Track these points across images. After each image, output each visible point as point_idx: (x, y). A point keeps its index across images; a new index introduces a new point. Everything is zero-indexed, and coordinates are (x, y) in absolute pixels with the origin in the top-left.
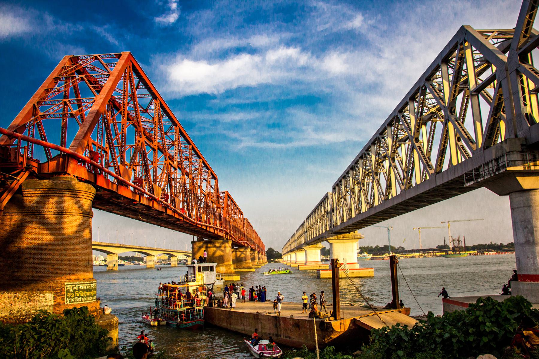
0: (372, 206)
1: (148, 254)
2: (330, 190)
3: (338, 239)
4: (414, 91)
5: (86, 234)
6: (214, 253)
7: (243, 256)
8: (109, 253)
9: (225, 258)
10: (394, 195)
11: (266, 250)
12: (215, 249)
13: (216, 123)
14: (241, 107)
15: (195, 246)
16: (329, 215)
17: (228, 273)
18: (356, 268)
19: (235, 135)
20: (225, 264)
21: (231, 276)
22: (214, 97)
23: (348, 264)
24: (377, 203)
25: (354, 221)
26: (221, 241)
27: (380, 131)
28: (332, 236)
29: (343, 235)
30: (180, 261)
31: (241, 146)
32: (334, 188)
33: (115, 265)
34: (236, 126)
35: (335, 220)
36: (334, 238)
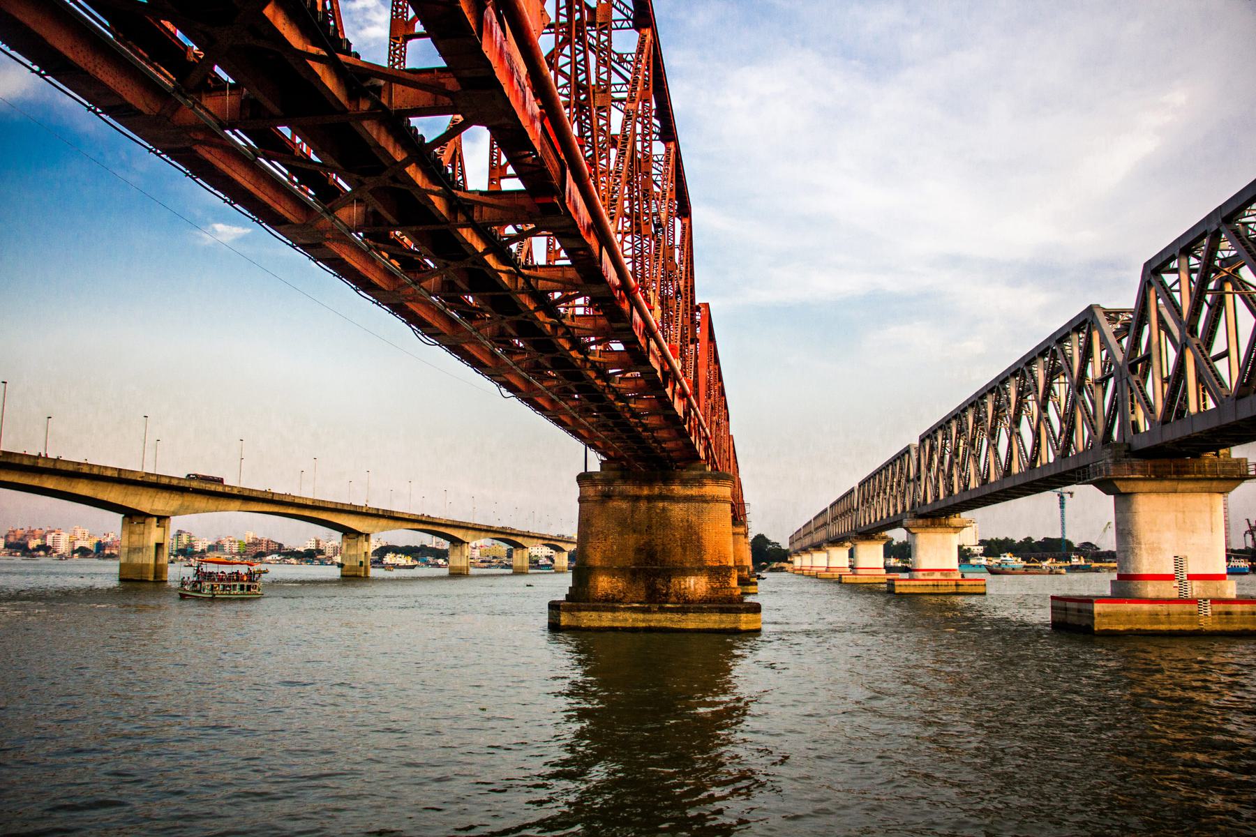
0: (985, 482)
1: (456, 542)
2: (916, 442)
4: (1191, 238)
10: (1045, 461)
11: (751, 536)
16: (912, 485)
17: (720, 601)
23: (1192, 577)
24: (992, 479)
25: (943, 505)
27: (1155, 265)
29: (1179, 462)
30: (537, 562)
32: (922, 440)
35: (922, 494)
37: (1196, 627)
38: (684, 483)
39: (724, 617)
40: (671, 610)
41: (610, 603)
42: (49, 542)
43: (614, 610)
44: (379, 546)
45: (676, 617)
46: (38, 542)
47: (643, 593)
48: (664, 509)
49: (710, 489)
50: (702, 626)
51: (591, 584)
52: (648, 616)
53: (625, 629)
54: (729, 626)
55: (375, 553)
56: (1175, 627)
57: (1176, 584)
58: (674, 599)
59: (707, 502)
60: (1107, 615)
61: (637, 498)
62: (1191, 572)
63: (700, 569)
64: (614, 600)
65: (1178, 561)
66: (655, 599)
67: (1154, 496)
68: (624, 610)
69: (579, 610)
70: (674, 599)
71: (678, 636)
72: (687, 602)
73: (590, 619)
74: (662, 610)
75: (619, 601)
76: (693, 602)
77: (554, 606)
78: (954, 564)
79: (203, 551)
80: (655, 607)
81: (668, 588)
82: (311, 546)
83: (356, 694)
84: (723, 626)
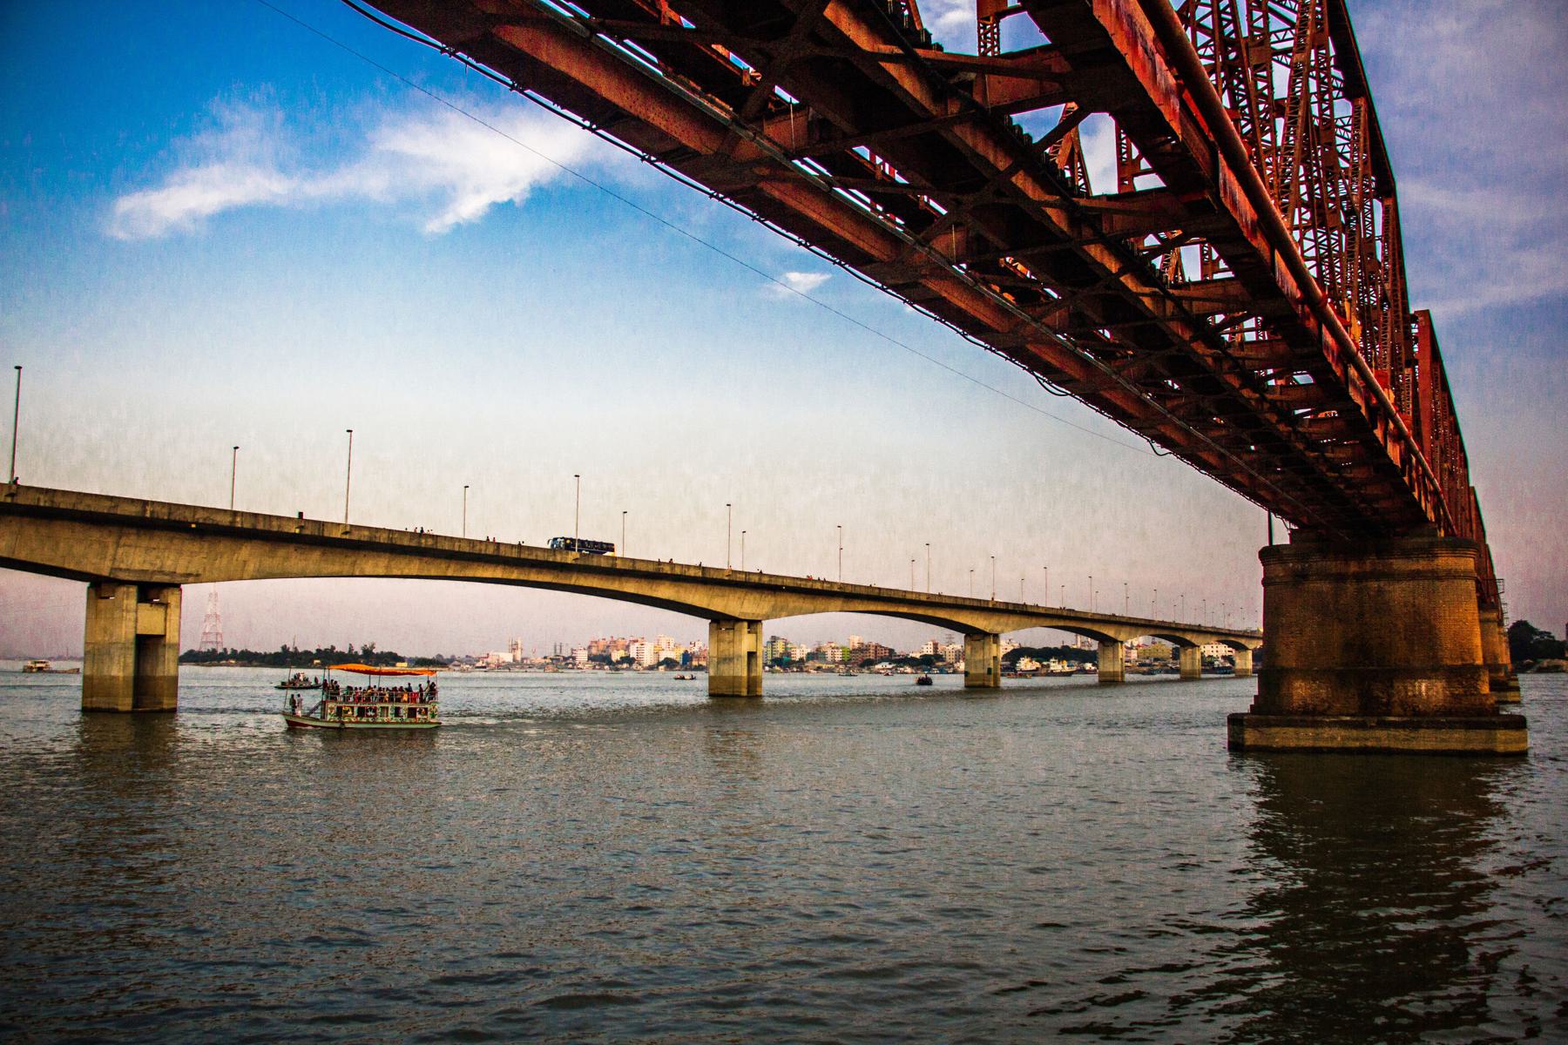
38: (1407, 554)
39: (1472, 734)
41: (1309, 716)
44: (1010, 648)
45: (1402, 733)
48: (1380, 591)
49: (1445, 561)
53: (1331, 750)
54: (1477, 746)
55: (1006, 657)
59: (1439, 579)
61: (1341, 578)
63: (1433, 669)
66: (1371, 711)
70: (1399, 710)
72: (1416, 713)
75: (1323, 713)
76: (1425, 714)
81: (1390, 696)
82: (929, 651)
84: (1470, 747)
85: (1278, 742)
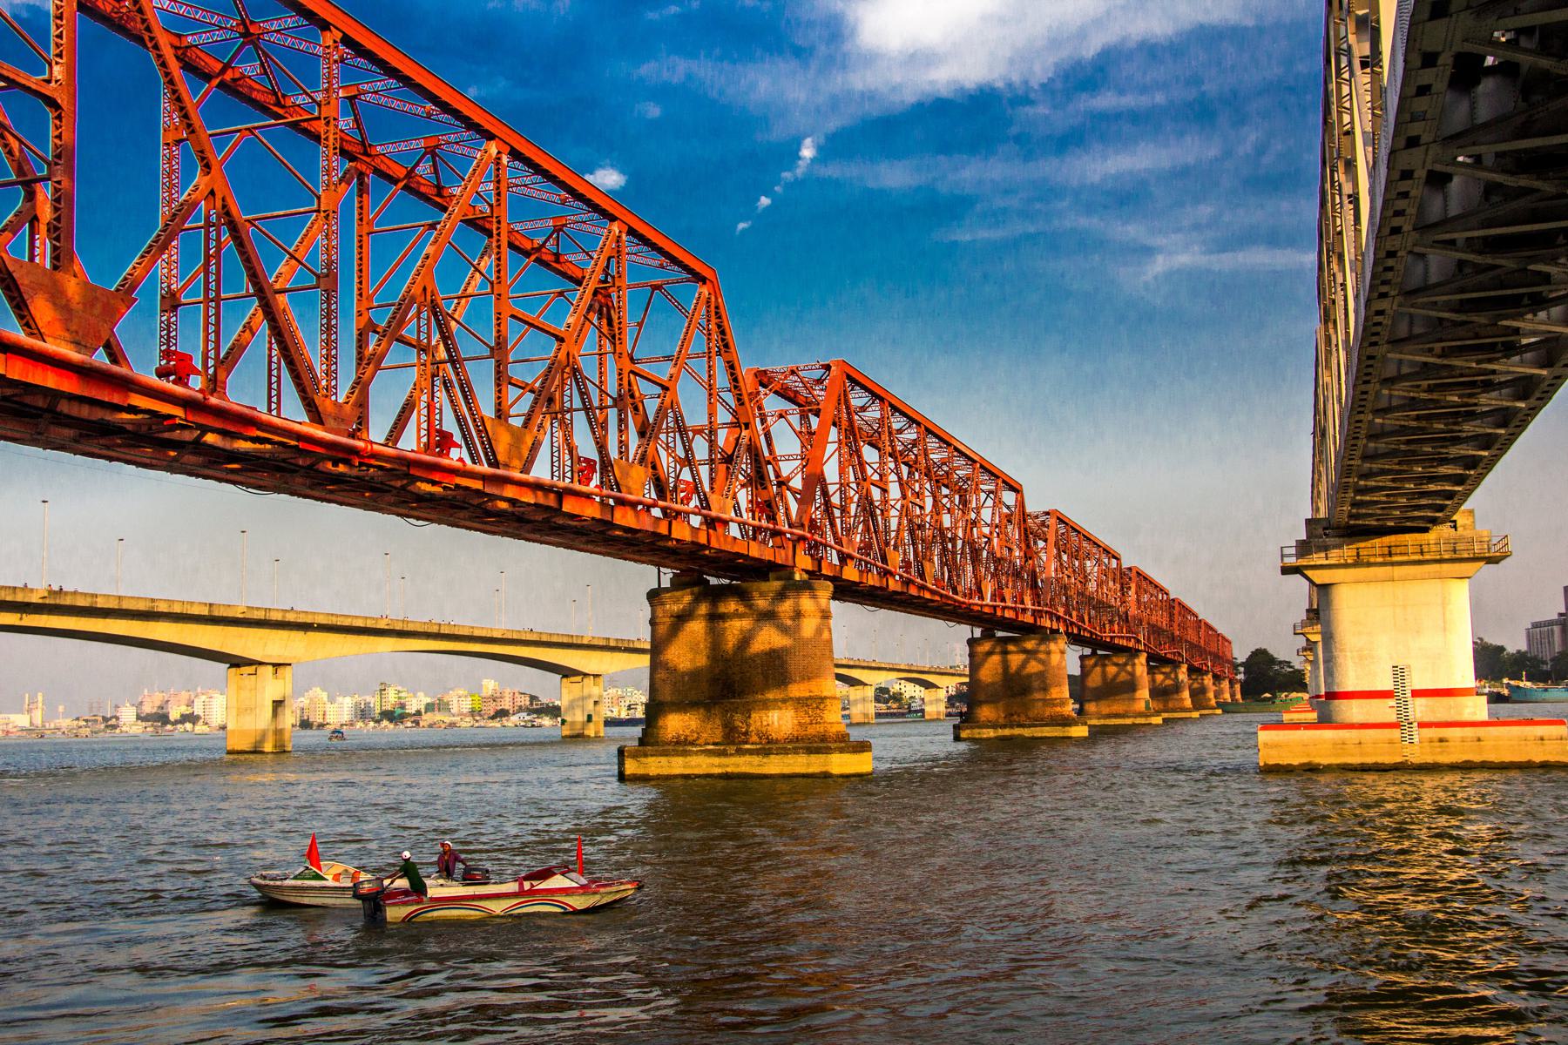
3: (1358, 563)
5: (825, 635)
6: (745, 641)
7: (1034, 667)
8: (566, 673)
9: (794, 664)
12: (1022, 657)
13: (1049, 192)
14: (1143, 123)
15: (660, 613)
17: (810, 739)
18: (1467, 716)
19: (1133, 231)
20: (796, 690)
21: (818, 751)
22: (1021, 97)
23: (1416, 693)
26: (777, 585)
28: (1326, 549)
31: (1159, 265)
33: (590, 718)
34: (1127, 198)
36: (1335, 556)
37: (1399, 760)
39: (813, 757)
40: (751, 752)
41: (681, 746)
42: (198, 710)
43: (685, 753)
45: (756, 759)
46: (184, 710)
47: (718, 737)
50: (787, 770)
51: (661, 723)
52: (724, 760)
56: (1370, 760)
57: (1392, 702)
58: (755, 738)
60: (1276, 746)
62: (1419, 685)
64: (686, 742)
65: (1399, 672)
67: (1362, 587)
68: (696, 753)
69: (646, 756)
70: (755, 738)
71: (753, 784)
72: (770, 741)
73: (656, 765)
74: (740, 752)
75: (692, 744)
76: (777, 741)
77: (621, 752)
78: (1463, 673)
79: (418, 713)
80: (732, 749)
81: (748, 726)
83: (373, 846)
84: (811, 770)
85: (653, 771)
